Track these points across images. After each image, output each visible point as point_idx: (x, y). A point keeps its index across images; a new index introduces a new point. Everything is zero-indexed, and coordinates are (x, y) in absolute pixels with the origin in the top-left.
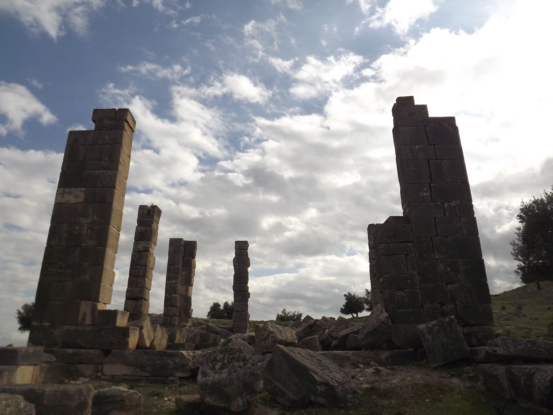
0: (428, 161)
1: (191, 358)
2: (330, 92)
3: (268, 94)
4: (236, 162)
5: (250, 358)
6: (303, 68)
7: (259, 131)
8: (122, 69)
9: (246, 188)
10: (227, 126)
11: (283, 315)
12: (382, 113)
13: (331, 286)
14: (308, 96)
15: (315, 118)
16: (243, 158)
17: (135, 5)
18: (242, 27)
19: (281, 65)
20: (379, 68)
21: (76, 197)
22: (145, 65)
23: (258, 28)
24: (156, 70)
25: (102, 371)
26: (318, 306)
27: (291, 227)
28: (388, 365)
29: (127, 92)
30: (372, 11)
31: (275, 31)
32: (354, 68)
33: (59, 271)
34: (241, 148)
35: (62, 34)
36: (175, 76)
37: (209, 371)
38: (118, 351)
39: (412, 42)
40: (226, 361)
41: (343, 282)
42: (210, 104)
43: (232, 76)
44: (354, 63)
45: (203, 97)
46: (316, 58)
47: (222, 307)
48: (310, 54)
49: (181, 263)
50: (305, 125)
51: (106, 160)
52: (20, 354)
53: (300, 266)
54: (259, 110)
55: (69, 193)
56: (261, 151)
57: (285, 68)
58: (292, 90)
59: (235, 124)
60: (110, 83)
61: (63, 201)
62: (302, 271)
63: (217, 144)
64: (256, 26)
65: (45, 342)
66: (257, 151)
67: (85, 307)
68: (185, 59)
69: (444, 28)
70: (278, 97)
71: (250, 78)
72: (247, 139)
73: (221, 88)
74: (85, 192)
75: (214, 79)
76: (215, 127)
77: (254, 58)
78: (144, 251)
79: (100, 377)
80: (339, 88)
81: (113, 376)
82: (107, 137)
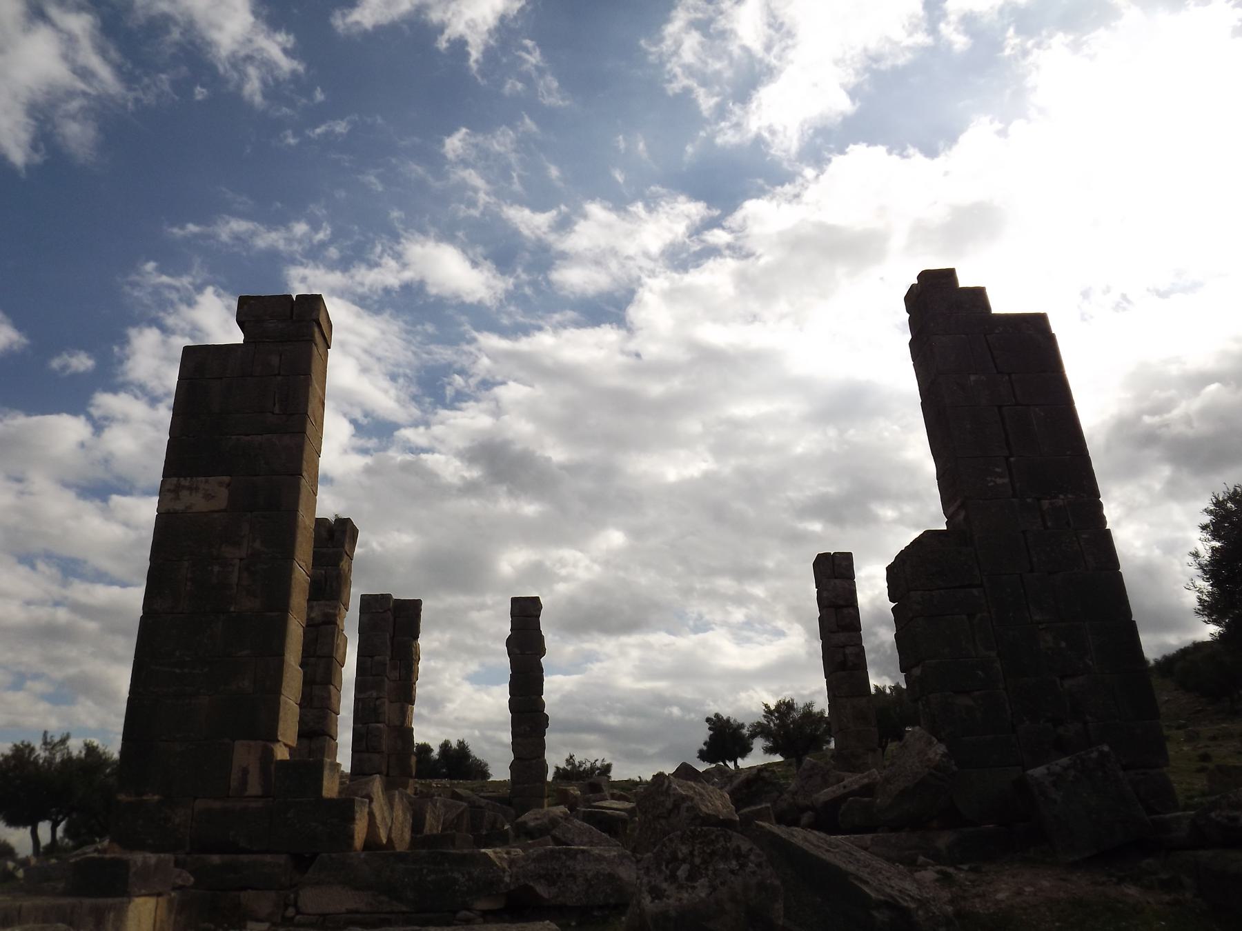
0: (1000, 407)
1: (505, 865)
2: (639, 278)
3: (503, 284)
4: (437, 430)
5: (751, 850)
6: (577, 228)
7: (485, 362)
8: (175, 230)
9: (470, 488)
10: (415, 353)
11: (569, 768)
12: (752, 322)
13: (662, 701)
14: (591, 290)
15: (609, 335)
16: (452, 421)
17: (199, 97)
18: (441, 143)
19: (531, 222)
20: (743, 228)
21: (208, 497)
22: (228, 223)
23: (476, 146)
24: (253, 234)
25: (295, 905)
26: (633, 746)
27: (563, 572)
28: (962, 863)
29: (185, 281)
30: (721, 112)
31: (515, 151)
32: (688, 228)
33: (177, 671)
34: (448, 401)
35: (38, 159)
36: (296, 247)
37: (665, 885)
38: (334, 855)
39: (809, 173)
40: (697, 861)
41: (687, 692)
42: (376, 306)
43: (423, 246)
44: (688, 216)
45: (360, 290)
46: (605, 208)
47: (436, 753)
48: (592, 198)
49: (389, 653)
50: (589, 348)
51: (277, 411)
52: (133, 870)
53: (591, 657)
54: (483, 318)
56: (492, 405)
57: (538, 228)
58: (556, 276)
59: (433, 347)
60: (147, 260)
61: (179, 506)
62: (596, 668)
63: (393, 392)
64: (473, 140)
65: (150, 841)
66: (483, 405)
67: (244, 755)
68: (319, 210)
69: (876, 144)
70: (528, 290)
71: (464, 251)
72: (458, 380)
73: (398, 272)
74: (229, 485)
75: (383, 251)
76: (387, 354)
77: (468, 207)
78: (324, 623)
79: (293, 918)
80: (658, 270)
81: (324, 915)
82: (275, 360)
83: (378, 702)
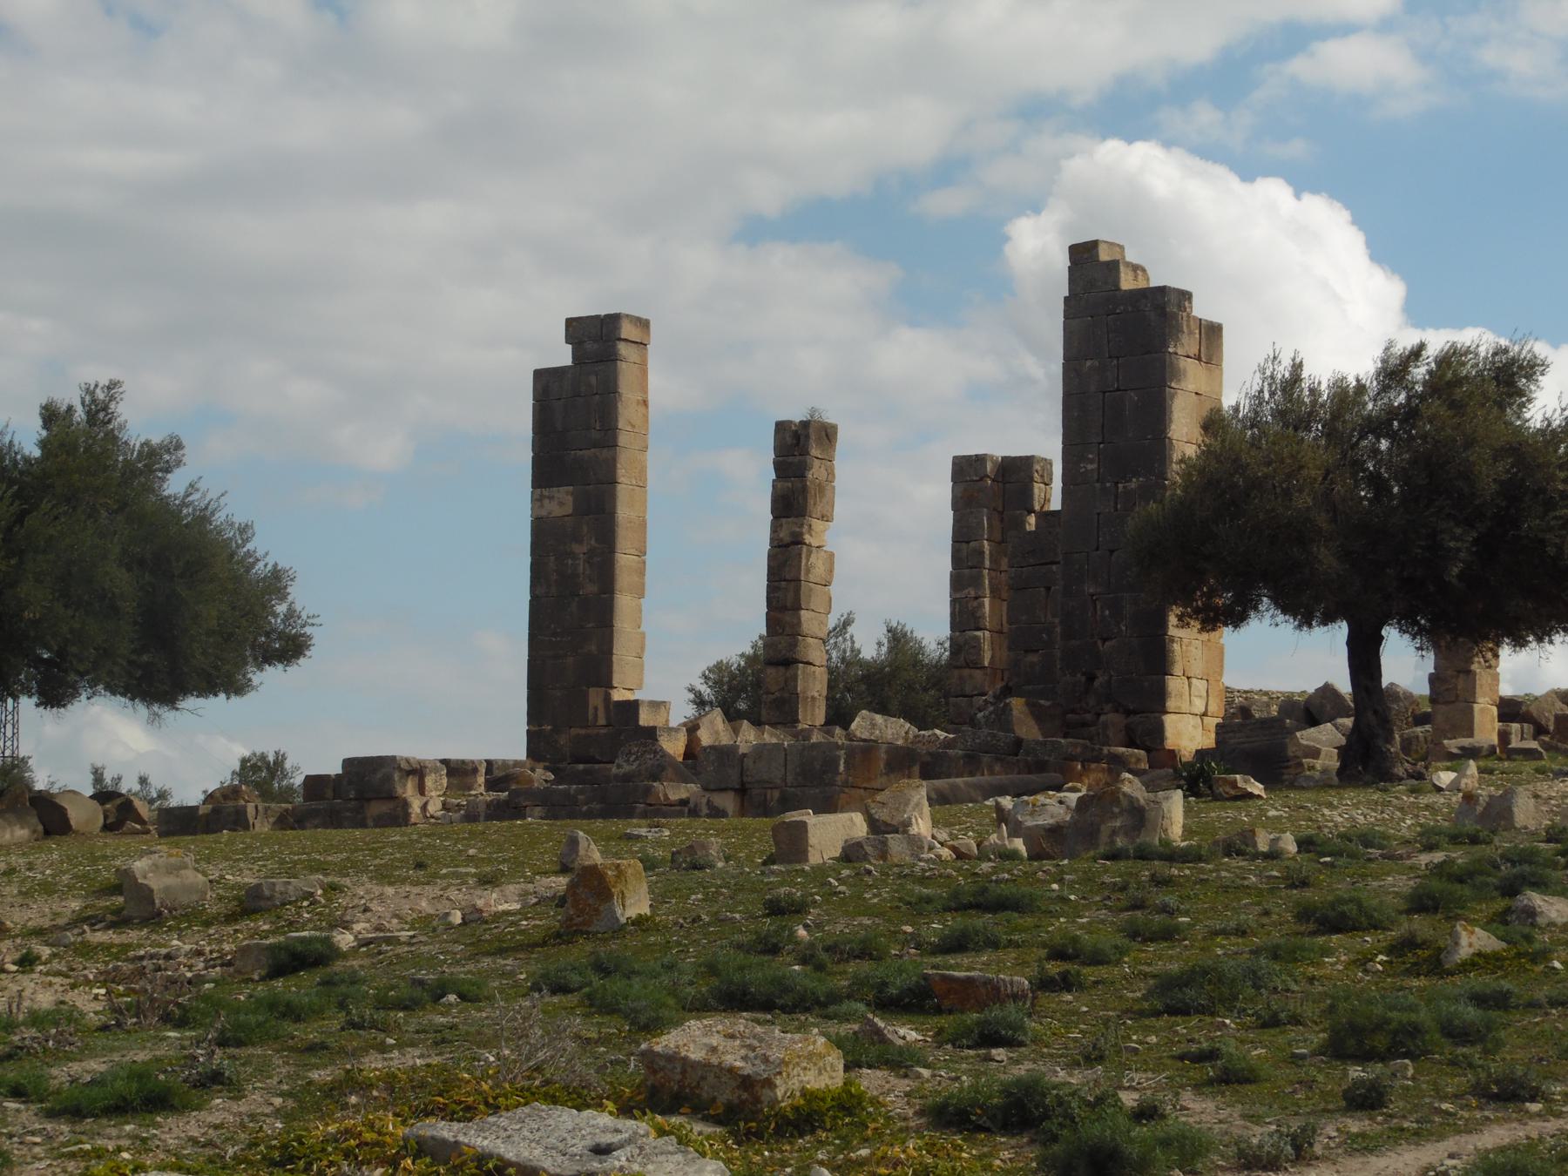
21: (561, 504)
55: (551, 498)
61: (544, 513)
67: (595, 697)
82: (593, 380)
83: (975, 604)
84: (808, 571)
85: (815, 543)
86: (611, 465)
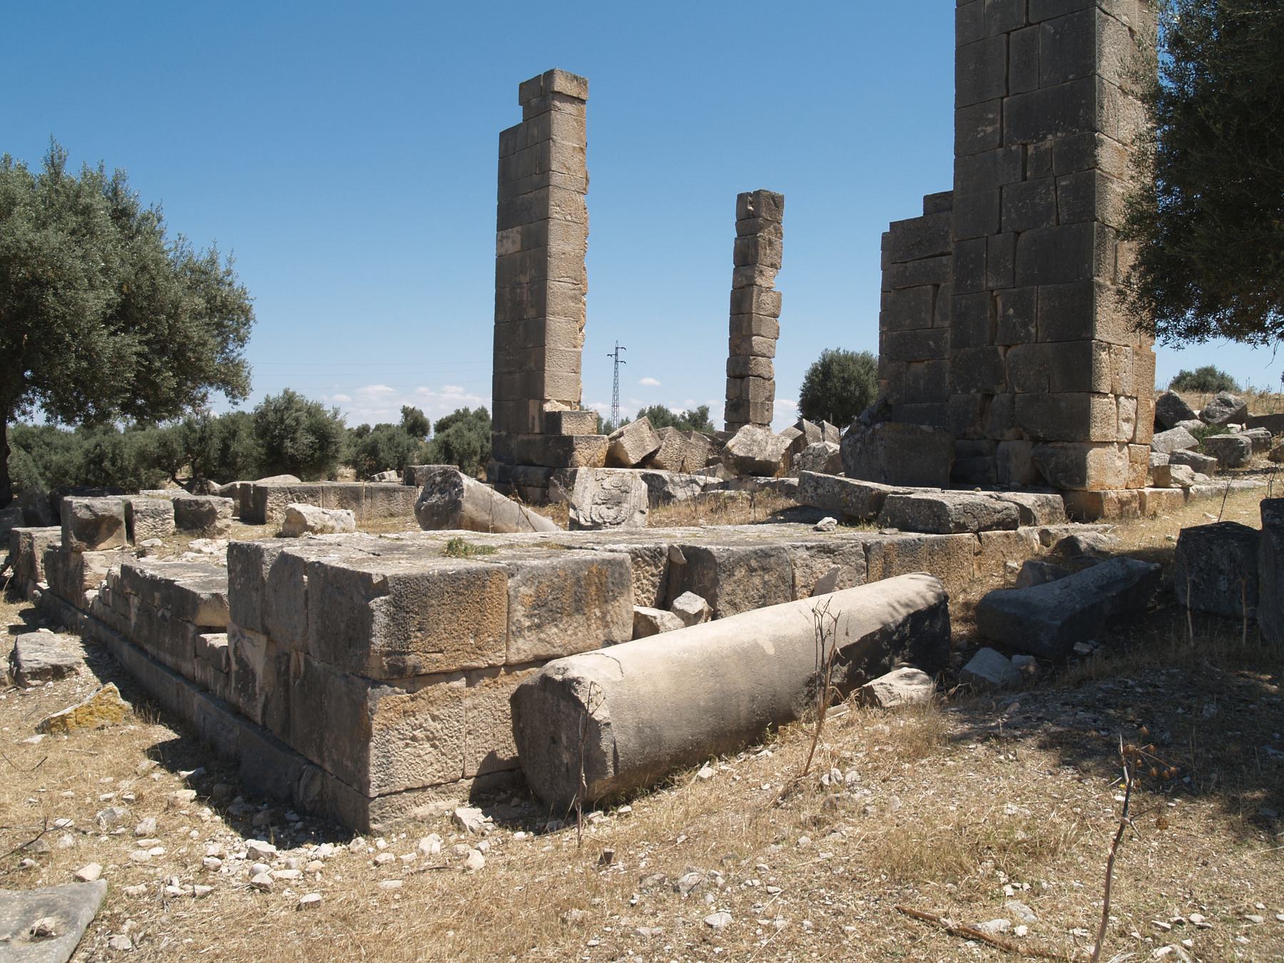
61: (503, 251)
67: (533, 405)
84: (759, 307)
85: (765, 284)
86: (544, 203)
